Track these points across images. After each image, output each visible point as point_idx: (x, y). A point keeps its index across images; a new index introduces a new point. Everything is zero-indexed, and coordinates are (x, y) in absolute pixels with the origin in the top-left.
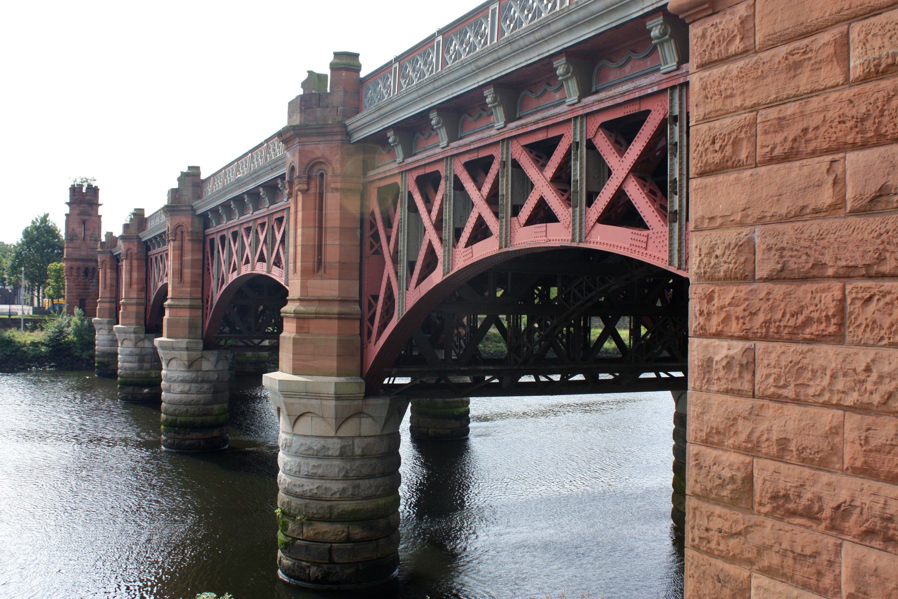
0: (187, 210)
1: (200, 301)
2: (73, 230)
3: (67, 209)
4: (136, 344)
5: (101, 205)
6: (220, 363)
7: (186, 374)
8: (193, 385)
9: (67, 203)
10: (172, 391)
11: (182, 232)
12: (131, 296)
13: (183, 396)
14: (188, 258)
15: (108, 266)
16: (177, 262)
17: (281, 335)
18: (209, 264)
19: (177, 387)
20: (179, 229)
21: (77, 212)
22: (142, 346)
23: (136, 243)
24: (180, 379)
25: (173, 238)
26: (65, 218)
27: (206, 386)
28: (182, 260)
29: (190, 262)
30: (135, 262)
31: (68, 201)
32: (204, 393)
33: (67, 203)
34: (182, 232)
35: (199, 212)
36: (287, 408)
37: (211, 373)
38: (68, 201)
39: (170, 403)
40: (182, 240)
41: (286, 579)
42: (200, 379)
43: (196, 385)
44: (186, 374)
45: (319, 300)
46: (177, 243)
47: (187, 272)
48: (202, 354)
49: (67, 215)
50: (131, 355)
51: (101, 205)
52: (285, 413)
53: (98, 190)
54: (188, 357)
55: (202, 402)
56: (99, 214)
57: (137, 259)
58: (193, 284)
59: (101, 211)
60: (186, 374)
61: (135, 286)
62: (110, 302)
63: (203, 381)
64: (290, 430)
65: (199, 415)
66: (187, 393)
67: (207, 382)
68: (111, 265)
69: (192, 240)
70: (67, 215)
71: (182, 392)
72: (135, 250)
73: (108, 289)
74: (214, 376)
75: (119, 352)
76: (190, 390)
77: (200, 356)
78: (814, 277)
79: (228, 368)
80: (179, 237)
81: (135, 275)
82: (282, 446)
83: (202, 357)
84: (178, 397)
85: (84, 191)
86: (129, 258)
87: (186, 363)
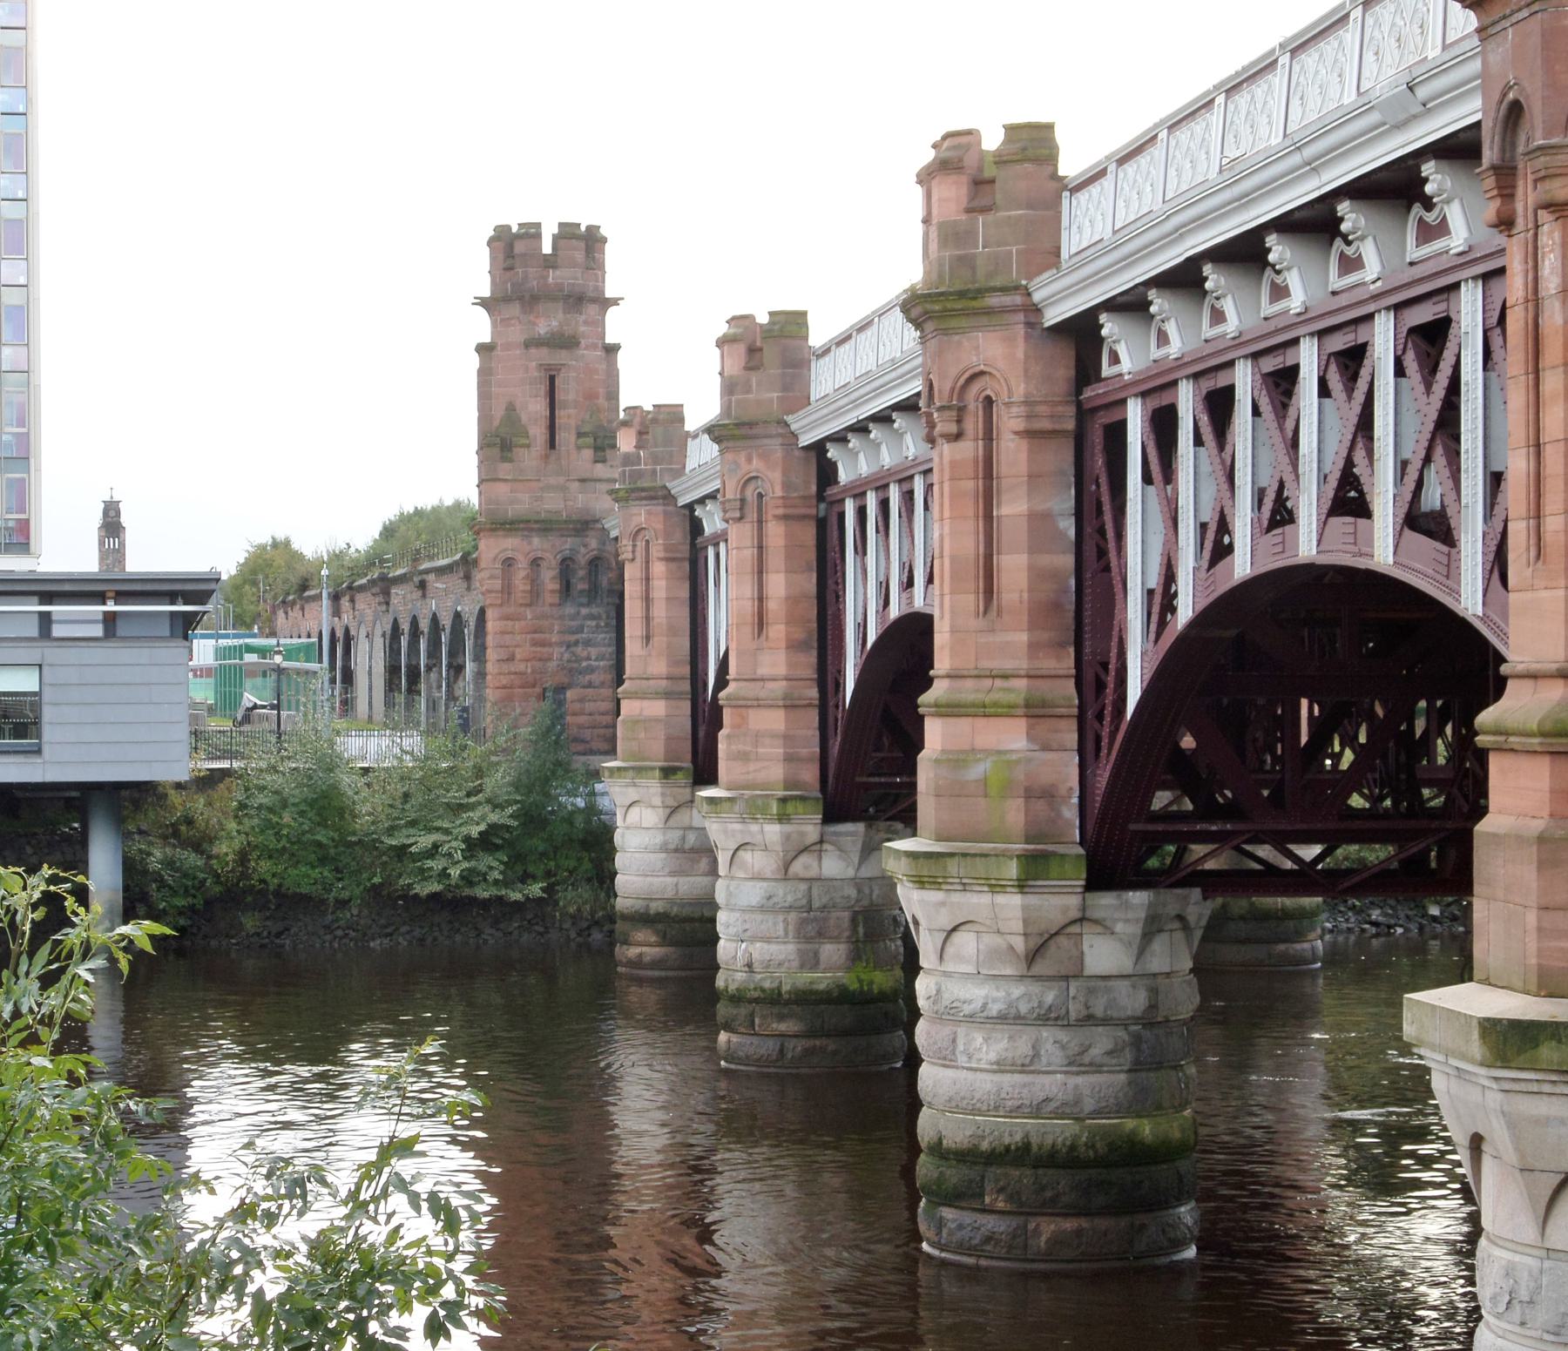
0: (1004, 310)
1: (1071, 683)
2: (511, 408)
3: (481, 327)
4: (787, 866)
5: (615, 302)
6: (1159, 945)
7: (1017, 991)
8: (1046, 1033)
9: (484, 303)
10: (962, 1060)
11: (989, 402)
12: (763, 671)
13: (1007, 1080)
14: (1013, 508)
15: (657, 551)
16: (969, 525)
17: (1482, 827)
18: (1101, 531)
19: (986, 1047)
20: (975, 389)
21: (517, 334)
22: (813, 873)
23: (779, 454)
24: (994, 1009)
25: (953, 428)
26: (474, 361)
27: (1101, 1042)
28: (988, 517)
29: (1023, 525)
30: (776, 533)
31: (486, 293)
32: (1095, 1067)
33: (484, 303)
34: (989, 402)
35: (1053, 316)
36: (1517, 1140)
37: (1123, 985)
38: (486, 293)
39: (955, 1106)
40: (989, 436)
41: (935, 1252)
42: (1075, 1010)
43: (1063, 1036)
44: (1019, 994)
45: (760, 572)
46: (968, 449)
47: (1014, 568)
48: (1084, 908)
49: (482, 349)
50: (765, 908)
51: (615, 302)
52: (1511, 1156)
53: (604, 240)
54: (1026, 922)
55: (1089, 1105)
56: (609, 339)
57: (785, 518)
58: (1041, 613)
59: (615, 327)
60: (1019, 994)
61: (777, 631)
62: (668, 695)
63: (1089, 1020)
64: (1530, 1233)
65: (1015, 1111)
66: (1023, 1069)
67: (1106, 1021)
68: (667, 548)
69: (1029, 434)
70: (482, 349)
71: (1001, 1067)
72: (773, 483)
73: (659, 641)
74: (1133, 1001)
75: (720, 897)
76: (1036, 1056)
77: (1074, 914)
78: (1493, 505)
79: (1190, 965)
80: (974, 424)
81: (777, 585)
82: (1494, 1298)
83: (1082, 920)
84: (985, 1084)
85: (547, 249)
86: (752, 515)
87: (1019, 944)
